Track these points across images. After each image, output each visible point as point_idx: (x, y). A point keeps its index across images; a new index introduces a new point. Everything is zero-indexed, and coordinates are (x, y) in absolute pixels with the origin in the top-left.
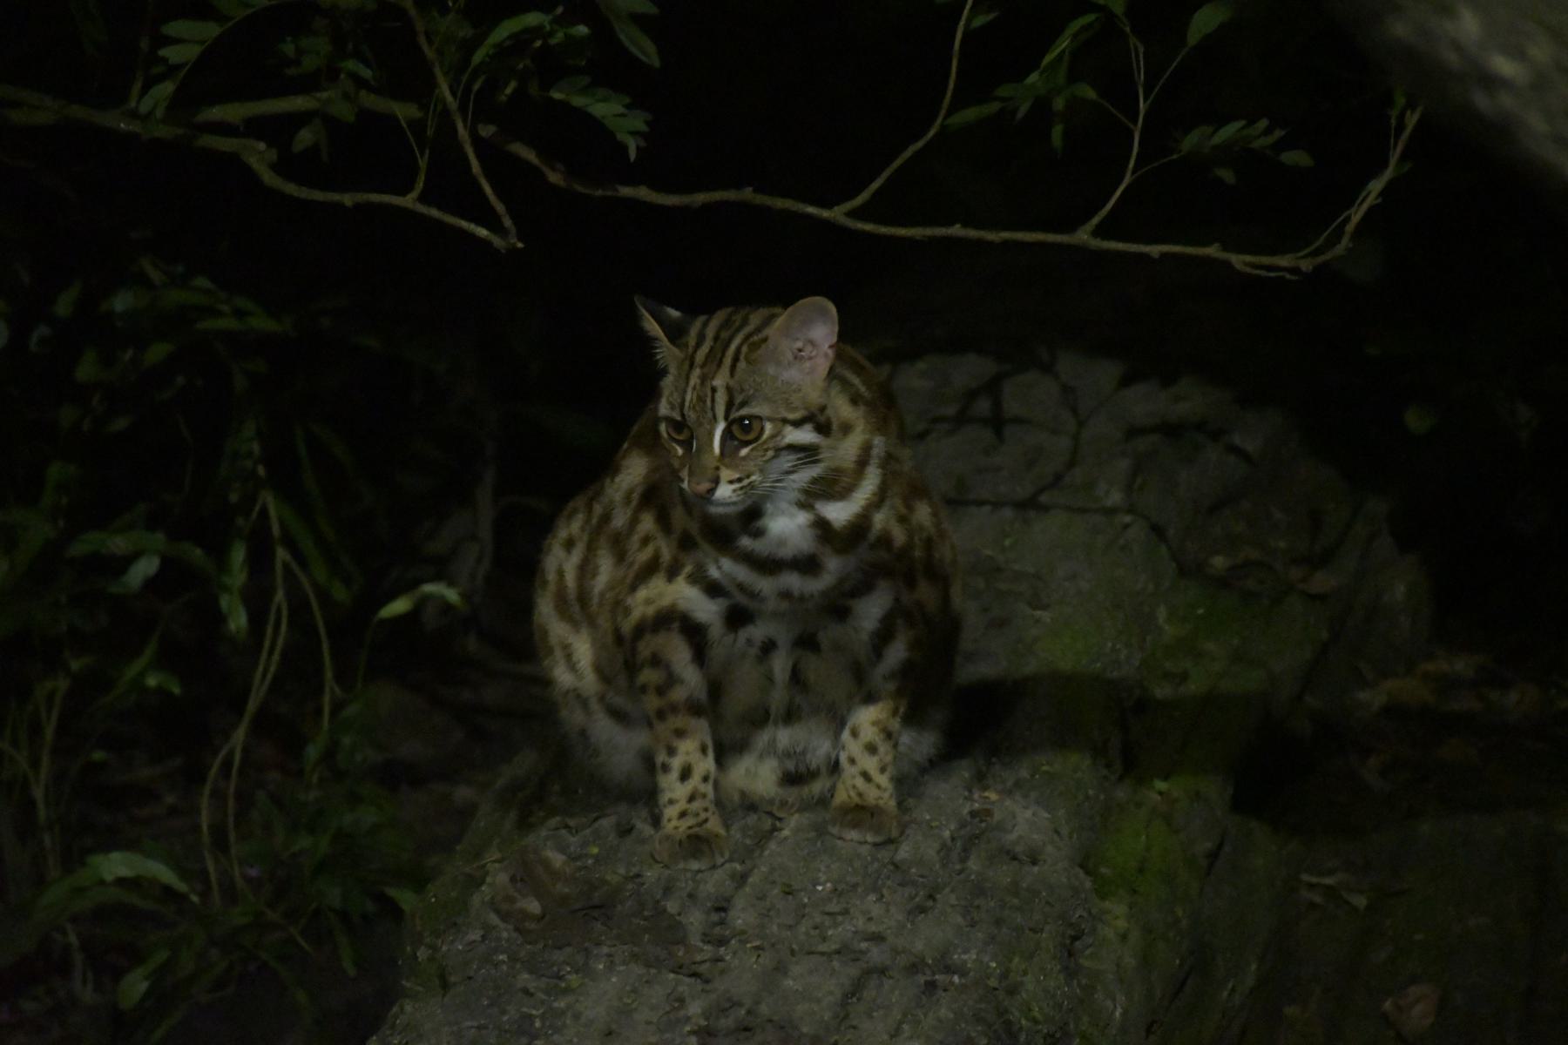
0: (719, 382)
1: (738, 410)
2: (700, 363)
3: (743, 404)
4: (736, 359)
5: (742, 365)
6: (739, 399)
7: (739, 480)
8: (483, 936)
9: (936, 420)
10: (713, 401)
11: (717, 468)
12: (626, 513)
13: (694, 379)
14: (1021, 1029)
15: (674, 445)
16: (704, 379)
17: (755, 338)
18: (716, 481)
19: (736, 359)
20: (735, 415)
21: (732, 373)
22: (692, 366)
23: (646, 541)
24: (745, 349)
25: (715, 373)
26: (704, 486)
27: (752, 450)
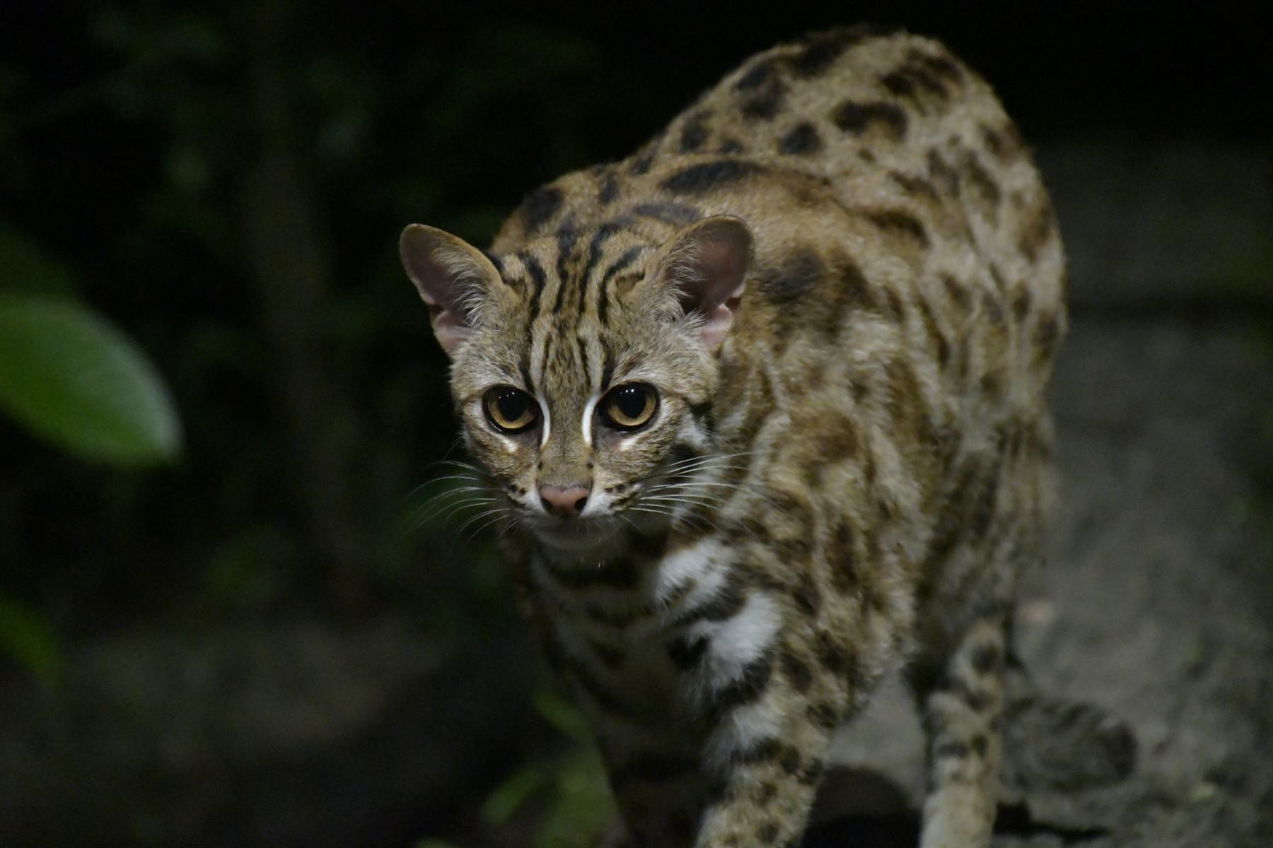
0: (589, 328)
1: (626, 372)
2: (551, 307)
3: (631, 365)
4: (603, 303)
5: (615, 312)
6: (624, 358)
7: (620, 488)
8: (715, 394)
9: (615, 244)
10: (584, 358)
11: (590, 466)
12: (665, 380)
13: (544, 326)
14: (798, 424)
15: (500, 436)
16: (562, 328)
17: (624, 272)
18: (589, 485)
19: (603, 303)
20: (619, 379)
21: (603, 316)
22: (534, 312)
23: (615, 458)
24: (611, 287)
25: (578, 320)
26: (572, 495)
27: (639, 442)
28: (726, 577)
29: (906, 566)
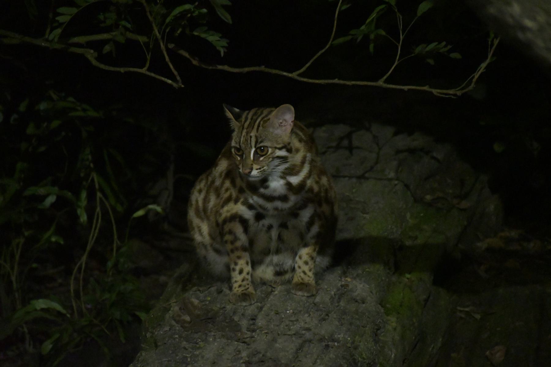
0: (253, 134)
1: (259, 144)
3: (261, 142)
4: (259, 126)
5: (261, 128)
6: (260, 140)
7: (260, 169)
9: (329, 148)
10: (251, 141)
11: (252, 165)
13: (244, 133)
15: (237, 156)
16: (247, 133)
17: (265, 119)
18: (252, 169)
19: (259, 126)
20: (258, 146)
21: (257, 131)
22: (243, 128)
23: (227, 190)
24: (262, 123)
25: (251, 131)
26: (247, 171)
27: (264, 158)
28: (275, 272)
29: (206, 37)
